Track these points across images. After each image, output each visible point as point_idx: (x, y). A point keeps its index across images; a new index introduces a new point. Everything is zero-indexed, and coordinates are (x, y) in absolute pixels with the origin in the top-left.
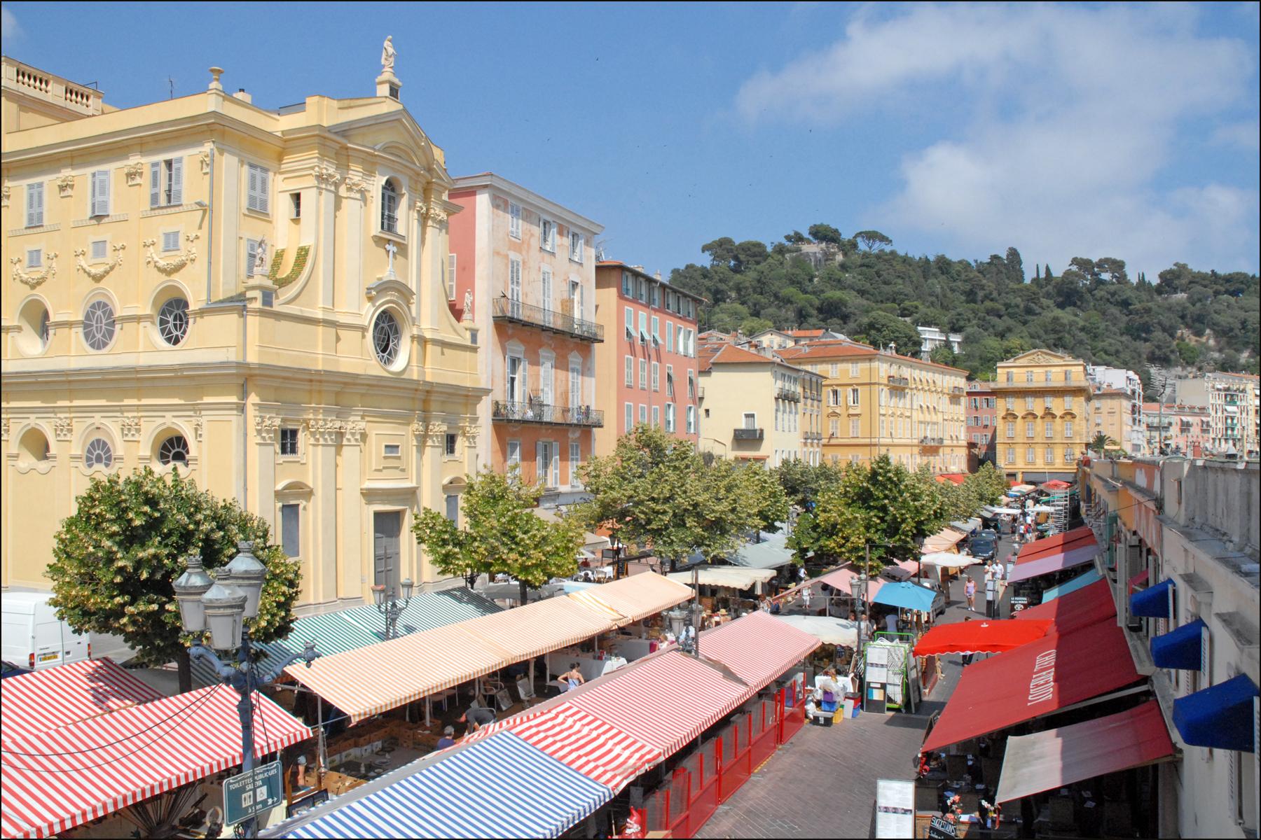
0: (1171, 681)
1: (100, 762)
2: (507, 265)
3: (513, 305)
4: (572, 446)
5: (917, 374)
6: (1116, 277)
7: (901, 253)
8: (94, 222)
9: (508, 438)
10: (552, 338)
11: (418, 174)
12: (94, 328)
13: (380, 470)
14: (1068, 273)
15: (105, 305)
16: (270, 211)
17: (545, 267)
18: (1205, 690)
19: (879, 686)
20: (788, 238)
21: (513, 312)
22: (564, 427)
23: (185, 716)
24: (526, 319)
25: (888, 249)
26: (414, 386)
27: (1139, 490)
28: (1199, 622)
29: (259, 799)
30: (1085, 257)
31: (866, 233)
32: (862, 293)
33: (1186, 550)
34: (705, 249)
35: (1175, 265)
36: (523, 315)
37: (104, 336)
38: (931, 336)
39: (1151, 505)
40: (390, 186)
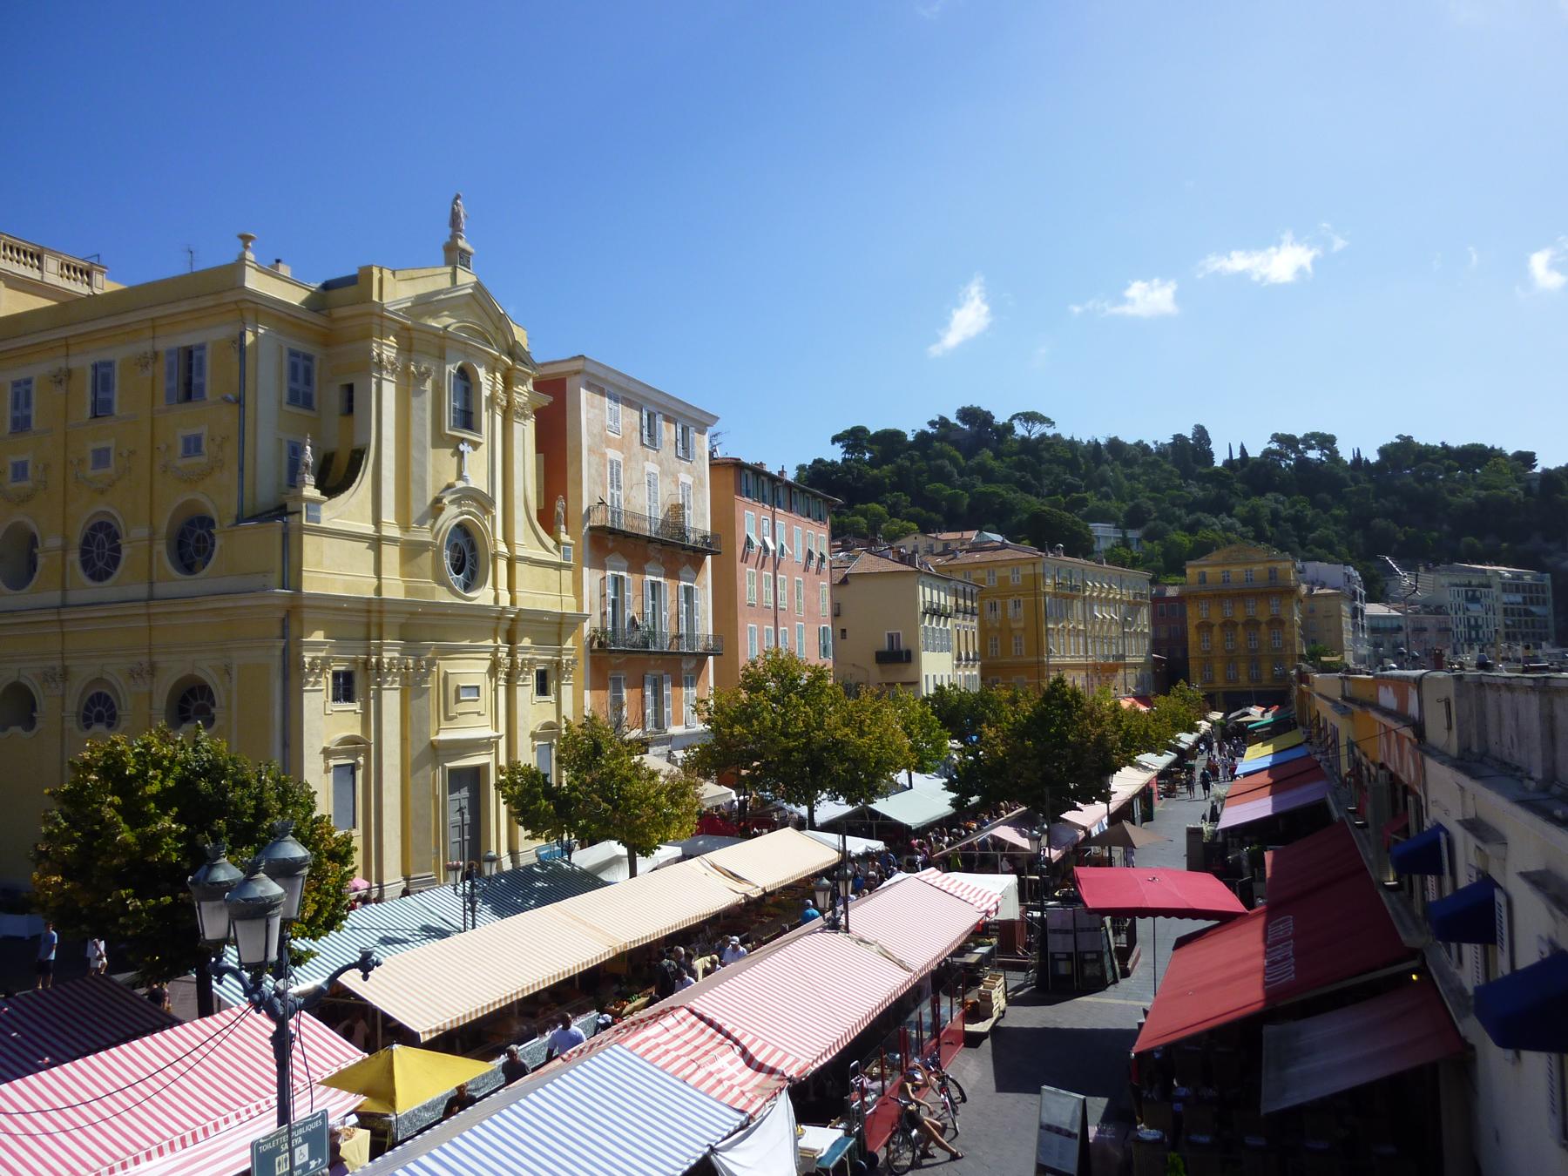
0: (1450, 955)
1: (82, 1123)
3: (613, 513)
4: (686, 678)
6: (1325, 455)
7: (1067, 437)
9: (610, 672)
10: (660, 550)
12: (95, 555)
14: (1267, 453)
15: (109, 526)
18: (1506, 978)
19: (1064, 956)
21: (613, 521)
22: (678, 657)
23: (191, 1063)
24: (629, 530)
25: (1050, 432)
27: (1387, 713)
28: (1486, 884)
29: (297, 1162)
30: (1287, 433)
33: (1462, 788)
35: (1398, 437)
37: (107, 564)
39: (1408, 732)
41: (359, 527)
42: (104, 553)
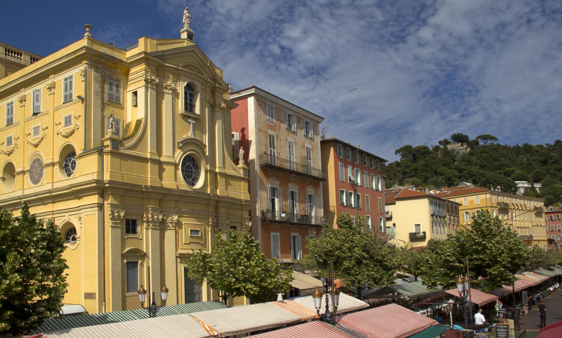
2: (267, 137)
5: (514, 201)
7: (503, 144)
8: (34, 117)
11: (207, 82)
13: (189, 244)
16: (121, 102)
17: (290, 139)
20: (440, 142)
25: (495, 143)
26: (208, 197)
31: (482, 136)
32: (482, 167)
34: (397, 152)
36: (277, 163)
37: (38, 177)
38: (522, 185)
40: (189, 88)
41: (139, 154)
42: (35, 170)
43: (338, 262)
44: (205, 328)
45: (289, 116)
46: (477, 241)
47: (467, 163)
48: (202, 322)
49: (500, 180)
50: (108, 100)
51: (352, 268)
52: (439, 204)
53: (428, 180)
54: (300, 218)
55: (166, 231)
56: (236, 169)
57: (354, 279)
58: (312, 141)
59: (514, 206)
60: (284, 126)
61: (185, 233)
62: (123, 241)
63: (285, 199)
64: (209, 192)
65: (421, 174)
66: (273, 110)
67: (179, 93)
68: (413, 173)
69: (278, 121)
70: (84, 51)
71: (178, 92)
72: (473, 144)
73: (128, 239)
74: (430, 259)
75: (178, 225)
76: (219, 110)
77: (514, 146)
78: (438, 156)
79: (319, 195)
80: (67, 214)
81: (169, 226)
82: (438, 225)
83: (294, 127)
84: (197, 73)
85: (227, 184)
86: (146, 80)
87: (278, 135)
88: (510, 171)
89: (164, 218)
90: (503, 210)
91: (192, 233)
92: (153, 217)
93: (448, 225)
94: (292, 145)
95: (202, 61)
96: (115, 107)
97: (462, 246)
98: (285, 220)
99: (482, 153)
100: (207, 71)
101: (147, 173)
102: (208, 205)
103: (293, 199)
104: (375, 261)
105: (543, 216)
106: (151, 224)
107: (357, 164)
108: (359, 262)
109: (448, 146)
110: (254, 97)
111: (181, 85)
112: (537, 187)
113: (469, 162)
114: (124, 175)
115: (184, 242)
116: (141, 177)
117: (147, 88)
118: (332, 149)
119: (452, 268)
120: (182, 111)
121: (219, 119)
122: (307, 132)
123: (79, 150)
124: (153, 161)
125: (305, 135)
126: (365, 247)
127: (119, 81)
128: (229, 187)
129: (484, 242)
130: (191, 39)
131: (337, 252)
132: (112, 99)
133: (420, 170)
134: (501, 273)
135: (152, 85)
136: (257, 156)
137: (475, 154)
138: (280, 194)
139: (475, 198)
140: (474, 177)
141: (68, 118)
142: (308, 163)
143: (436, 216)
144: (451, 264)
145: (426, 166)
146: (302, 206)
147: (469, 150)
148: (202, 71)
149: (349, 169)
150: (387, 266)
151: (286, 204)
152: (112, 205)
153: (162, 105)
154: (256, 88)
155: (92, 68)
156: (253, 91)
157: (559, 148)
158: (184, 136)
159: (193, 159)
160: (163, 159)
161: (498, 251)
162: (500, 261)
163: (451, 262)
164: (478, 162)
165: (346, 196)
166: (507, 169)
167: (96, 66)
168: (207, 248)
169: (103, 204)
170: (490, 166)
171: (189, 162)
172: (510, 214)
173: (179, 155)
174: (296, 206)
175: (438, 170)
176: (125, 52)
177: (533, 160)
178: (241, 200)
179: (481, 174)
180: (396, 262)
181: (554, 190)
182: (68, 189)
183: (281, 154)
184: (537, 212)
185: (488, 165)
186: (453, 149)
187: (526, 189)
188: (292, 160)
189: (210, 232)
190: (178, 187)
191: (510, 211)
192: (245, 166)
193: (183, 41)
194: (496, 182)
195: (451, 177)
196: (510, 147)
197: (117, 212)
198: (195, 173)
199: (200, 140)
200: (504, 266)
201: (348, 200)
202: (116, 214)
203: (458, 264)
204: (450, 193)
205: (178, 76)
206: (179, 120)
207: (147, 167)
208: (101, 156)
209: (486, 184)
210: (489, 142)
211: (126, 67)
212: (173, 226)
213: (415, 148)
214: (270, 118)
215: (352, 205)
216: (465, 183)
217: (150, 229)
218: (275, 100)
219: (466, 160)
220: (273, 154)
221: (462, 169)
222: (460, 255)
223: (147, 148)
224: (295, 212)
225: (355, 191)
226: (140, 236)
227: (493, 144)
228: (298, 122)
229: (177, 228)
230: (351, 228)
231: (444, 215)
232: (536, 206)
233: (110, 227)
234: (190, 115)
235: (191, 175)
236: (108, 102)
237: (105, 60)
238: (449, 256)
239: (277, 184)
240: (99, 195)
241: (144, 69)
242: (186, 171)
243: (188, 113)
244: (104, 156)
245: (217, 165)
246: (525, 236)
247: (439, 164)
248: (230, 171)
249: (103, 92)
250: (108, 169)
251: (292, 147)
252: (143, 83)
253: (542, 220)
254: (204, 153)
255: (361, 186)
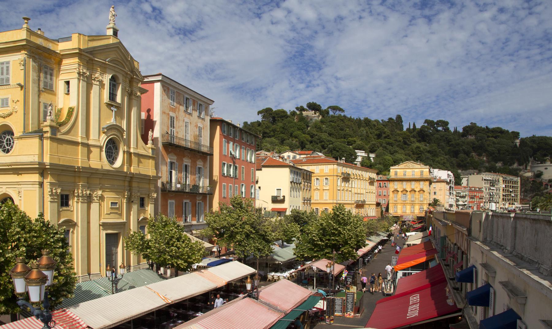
2: (169, 118)
5: (354, 171)
11: (127, 74)
16: (54, 89)
17: (186, 120)
25: (342, 114)
26: (125, 175)
32: (330, 135)
36: (176, 142)
38: (361, 154)
40: (113, 80)
41: (72, 138)
43: (232, 236)
44: (161, 298)
45: (187, 99)
46: (335, 227)
47: (318, 130)
48: (157, 293)
49: (344, 148)
50: (43, 88)
51: (243, 241)
52: (297, 172)
53: (285, 142)
54: (191, 187)
55: (92, 204)
56: (146, 149)
57: (244, 249)
58: (203, 121)
59: (354, 176)
60: (182, 108)
61: (106, 205)
62: (59, 213)
63: (180, 171)
64: (125, 170)
65: (279, 135)
66: (174, 95)
67: (104, 84)
68: (272, 133)
69: (178, 104)
70: (25, 43)
71: (104, 83)
72: (324, 113)
73: (63, 211)
74: (300, 237)
75: (102, 198)
76: (135, 98)
77: (357, 119)
78: (294, 120)
79: (206, 168)
80: (5, 187)
81: (94, 200)
82: (295, 190)
83: (190, 110)
84: (121, 67)
85: (139, 162)
86: (79, 73)
87: (178, 116)
88: (352, 141)
89: (91, 192)
90: (345, 179)
91: (112, 205)
92: (82, 192)
93: (302, 189)
94: (188, 125)
95: (124, 56)
96: (49, 93)
97: (324, 229)
98: (180, 190)
99: (331, 121)
100: (128, 64)
101: (78, 155)
102: (124, 181)
103: (186, 172)
104: (259, 235)
105: (375, 185)
106: (80, 199)
107: (237, 140)
108: (248, 236)
109: (303, 113)
110: (161, 83)
111: (106, 77)
112: (372, 157)
113: (320, 129)
114: (60, 157)
115: (106, 213)
116: (73, 159)
117: (79, 80)
118: (218, 127)
119: (316, 245)
120: (107, 100)
121: (135, 107)
122: (200, 113)
123: (18, 131)
124: (84, 145)
125: (198, 116)
126: (252, 224)
127: (52, 70)
128: (140, 164)
129: (339, 229)
130: (116, 36)
131: (232, 228)
132: (47, 86)
133: (278, 131)
134: (349, 252)
135: (84, 77)
136: (160, 135)
137: (325, 122)
138: (176, 168)
139: (325, 167)
140: (323, 143)
141: (5, 100)
142: (199, 140)
143: (294, 183)
144: (315, 242)
145: (283, 128)
146: (193, 177)
147: (320, 118)
148: (124, 65)
149: (231, 143)
150: (268, 239)
151: (181, 176)
152: (51, 184)
153: (91, 94)
154: (163, 75)
155: (30, 58)
156: (160, 78)
157: (391, 125)
158: (108, 122)
159: (113, 141)
160: (91, 142)
161: (349, 236)
162: (349, 243)
163: (316, 241)
164: (327, 130)
165: (227, 168)
166: (350, 139)
167: (34, 57)
168: (122, 216)
169: (43, 182)
170: (337, 135)
171: (110, 144)
172: (350, 182)
173: (103, 139)
174: (188, 177)
175: (294, 134)
176: (57, 43)
177: (370, 133)
178: (149, 176)
179: (329, 141)
180: (275, 236)
181: (384, 160)
182: (8, 166)
183: (179, 133)
184: (371, 181)
185: (335, 133)
186: (307, 116)
187: (363, 158)
188: (187, 139)
189: (125, 204)
190: (102, 167)
191: (351, 179)
192: (153, 146)
193: (108, 37)
194: (340, 150)
195: (304, 141)
196: (353, 119)
197: (55, 190)
198: (115, 153)
199: (120, 125)
200: (352, 247)
201: (228, 171)
202: (54, 191)
203: (320, 243)
204: (305, 160)
205: (104, 69)
206: (104, 108)
207: (78, 149)
208: (41, 140)
209: (333, 150)
210: (338, 113)
211: (59, 58)
212: (97, 200)
213: (275, 111)
214: (172, 102)
215: (231, 175)
216: (317, 153)
217: (80, 203)
218: (177, 86)
219: (317, 127)
220: (172, 134)
221: (314, 135)
222: (322, 235)
223: (78, 132)
224: (188, 183)
225: (234, 163)
226: (71, 209)
227: (340, 115)
228: (194, 105)
229: (100, 201)
230: (241, 207)
231: (300, 181)
232: (371, 177)
233: (49, 202)
234: (113, 104)
235: (112, 155)
236: (43, 90)
237: (42, 52)
238: (314, 236)
239: (174, 159)
240: (39, 174)
241: (77, 63)
242: (108, 152)
243: (112, 102)
244: (44, 140)
245: (132, 146)
246: (360, 201)
247: (295, 128)
248: (141, 152)
249: (39, 80)
250: (47, 153)
251: (188, 127)
252: (77, 75)
253: (373, 188)
254: (122, 136)
255: (239, 159)
